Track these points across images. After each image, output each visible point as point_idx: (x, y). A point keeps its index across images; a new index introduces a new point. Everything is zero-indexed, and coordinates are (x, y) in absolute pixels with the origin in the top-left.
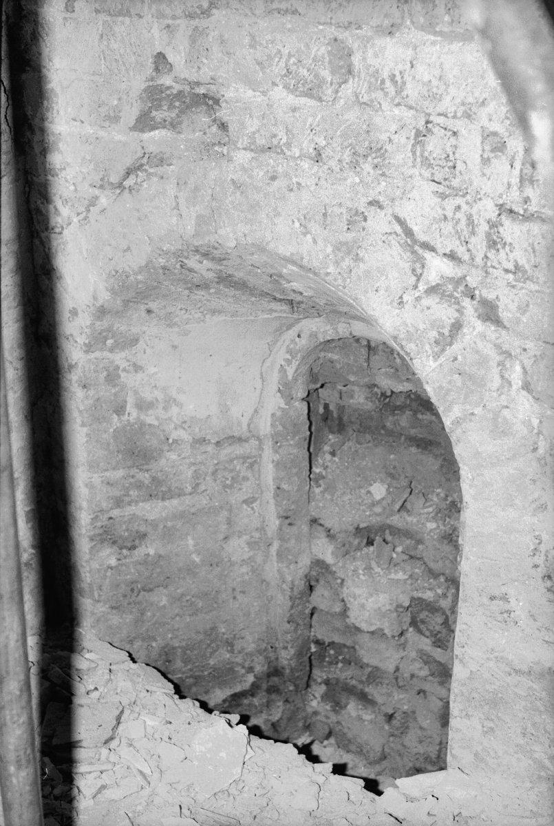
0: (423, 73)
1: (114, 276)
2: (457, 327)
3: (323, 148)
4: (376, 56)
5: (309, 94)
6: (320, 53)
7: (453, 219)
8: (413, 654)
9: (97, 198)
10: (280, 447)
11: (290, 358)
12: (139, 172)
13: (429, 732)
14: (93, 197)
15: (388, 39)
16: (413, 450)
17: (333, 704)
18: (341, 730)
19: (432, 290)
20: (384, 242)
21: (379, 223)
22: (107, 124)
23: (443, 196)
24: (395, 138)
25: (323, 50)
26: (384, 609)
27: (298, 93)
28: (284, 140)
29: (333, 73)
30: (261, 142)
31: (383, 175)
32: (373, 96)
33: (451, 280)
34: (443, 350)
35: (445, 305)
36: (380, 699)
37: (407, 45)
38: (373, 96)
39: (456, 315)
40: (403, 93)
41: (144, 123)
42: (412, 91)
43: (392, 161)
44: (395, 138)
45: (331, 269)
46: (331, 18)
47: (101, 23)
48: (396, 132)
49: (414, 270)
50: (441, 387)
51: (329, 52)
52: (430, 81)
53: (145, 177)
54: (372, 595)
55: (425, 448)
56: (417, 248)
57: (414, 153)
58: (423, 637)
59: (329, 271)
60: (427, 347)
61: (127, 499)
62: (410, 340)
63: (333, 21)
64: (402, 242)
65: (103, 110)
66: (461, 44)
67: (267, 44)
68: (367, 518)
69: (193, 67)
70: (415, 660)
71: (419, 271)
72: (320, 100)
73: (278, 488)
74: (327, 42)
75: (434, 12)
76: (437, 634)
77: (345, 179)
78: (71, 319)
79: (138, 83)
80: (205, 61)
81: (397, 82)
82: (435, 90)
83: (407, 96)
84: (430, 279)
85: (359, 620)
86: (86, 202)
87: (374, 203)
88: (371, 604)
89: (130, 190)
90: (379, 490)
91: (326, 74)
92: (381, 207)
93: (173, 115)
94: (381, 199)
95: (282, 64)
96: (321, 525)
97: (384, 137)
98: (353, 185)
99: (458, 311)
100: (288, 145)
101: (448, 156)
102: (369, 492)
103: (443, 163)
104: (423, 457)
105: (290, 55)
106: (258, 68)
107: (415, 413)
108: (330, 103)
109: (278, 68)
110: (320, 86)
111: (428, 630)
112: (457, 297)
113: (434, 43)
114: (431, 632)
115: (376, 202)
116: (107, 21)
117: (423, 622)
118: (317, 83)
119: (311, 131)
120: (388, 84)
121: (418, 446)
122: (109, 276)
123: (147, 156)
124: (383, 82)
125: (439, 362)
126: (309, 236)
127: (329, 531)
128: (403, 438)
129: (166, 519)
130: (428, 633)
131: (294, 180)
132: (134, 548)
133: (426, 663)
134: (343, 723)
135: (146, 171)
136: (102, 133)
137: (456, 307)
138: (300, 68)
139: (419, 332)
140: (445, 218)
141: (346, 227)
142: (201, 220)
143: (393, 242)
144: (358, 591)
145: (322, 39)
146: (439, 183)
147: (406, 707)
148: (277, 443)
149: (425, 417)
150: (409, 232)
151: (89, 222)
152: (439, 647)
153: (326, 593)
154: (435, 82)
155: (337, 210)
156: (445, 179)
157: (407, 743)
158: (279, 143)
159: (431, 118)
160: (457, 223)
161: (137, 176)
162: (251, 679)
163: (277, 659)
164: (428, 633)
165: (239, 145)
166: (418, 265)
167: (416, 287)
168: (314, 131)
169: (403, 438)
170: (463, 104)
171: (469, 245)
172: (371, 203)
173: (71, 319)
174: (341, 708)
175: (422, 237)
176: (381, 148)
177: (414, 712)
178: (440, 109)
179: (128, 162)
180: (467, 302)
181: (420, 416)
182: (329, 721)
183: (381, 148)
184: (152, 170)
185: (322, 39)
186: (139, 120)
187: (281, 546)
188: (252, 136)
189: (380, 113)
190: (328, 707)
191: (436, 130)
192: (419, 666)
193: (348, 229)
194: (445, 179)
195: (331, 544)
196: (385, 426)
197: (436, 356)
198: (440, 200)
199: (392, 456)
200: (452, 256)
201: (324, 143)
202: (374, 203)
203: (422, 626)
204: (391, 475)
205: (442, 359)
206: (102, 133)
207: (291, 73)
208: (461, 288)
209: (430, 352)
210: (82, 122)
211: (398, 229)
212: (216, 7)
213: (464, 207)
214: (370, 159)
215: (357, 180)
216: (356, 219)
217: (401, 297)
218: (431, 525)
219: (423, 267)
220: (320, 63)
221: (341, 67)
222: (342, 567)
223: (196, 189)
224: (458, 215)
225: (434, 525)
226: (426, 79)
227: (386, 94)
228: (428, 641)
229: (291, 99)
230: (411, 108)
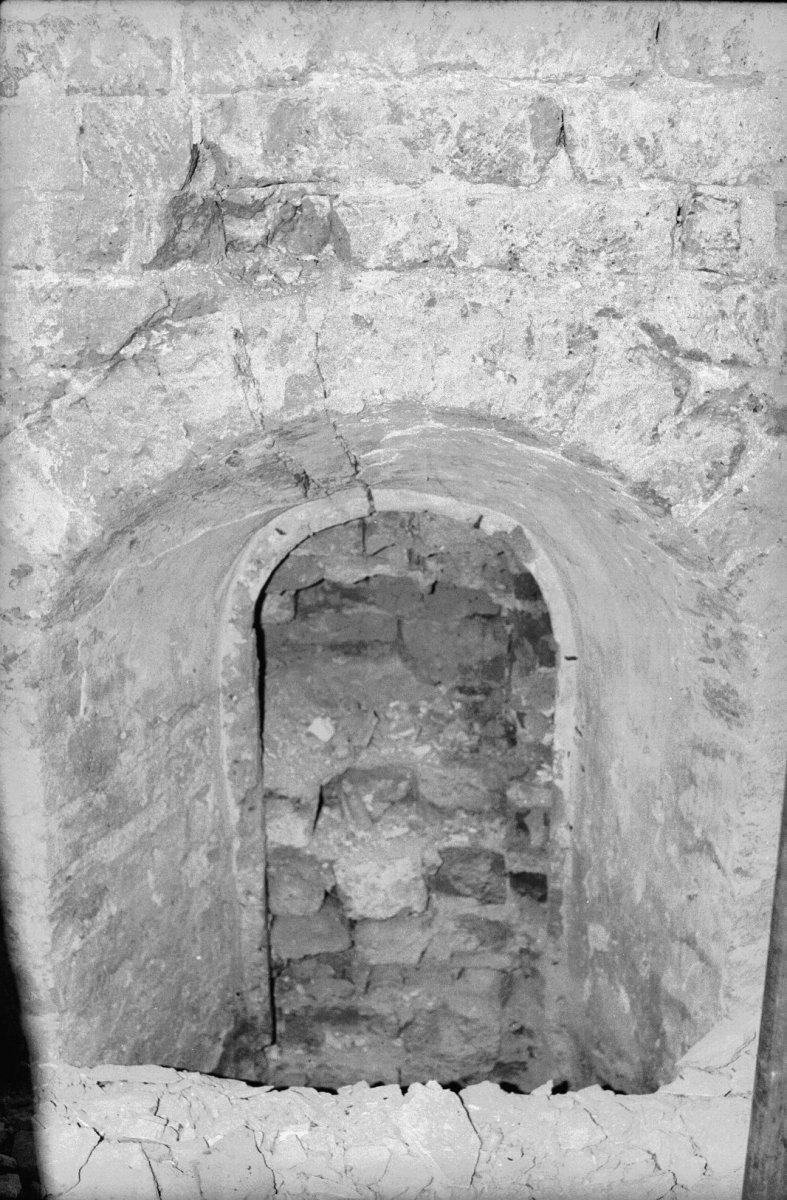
0: (687, 130)
1: (112, 497)
2: (739, 450)
3: (524, 250)
4: (613, 115)
5: (498, 178)
6: (518, 121)
7: (735, 314)
8: (451, 926)
9: (66, 383)
10: (236, 702)
11: (255, 569)
12: (153, 332)
13: (482, 1023)
14: (58, 384)
15: (632, 92)
16: (340, 661)
17: (304, 1045)
18: (326, 1074)
19: (700, 411)
20: (630, 360)
21: (614, 338)
22: (93, 266)
23: (718, 288)
24: (647, 222)
25: (523, 115)
26: (406, 880)
27: (478, 179)
28: (454, 247)
29: (536, 145)
30: (407, 254)
31: (623, 272)
32: (609, 170)
33: (723, 392)
34: (718, 485)
35: (719, 426)
36: (384, 1009)
37: (663, 98)
38: (609, 170)
39: (738, 435)
40: (657, 161)
41: (167, 255)
42: (671, 155)
43: (639, 253)
44: (647, 222)
45: (541, 412)
46: (537, 71)
47: (78, 109)
48: (648, 214)
49: (677, 389)
50: (716, 532)
51: (533, 118)
52: (699, 142)
53: (165, 338)
54: (384, 867)
55: (359, 653)
56: (678, 360)
57: (672, 236)
58: (463, 900)
59: (537, 415)
60: (696, 485)
61: (86, 840)
62: (666, 483)
63: (539, 75)
64: (656, 355)
65: (87, 246)
66: (745, 90)
67: (423, 114)
68: (324, 769)
69: (278, 160)
70: (455, 933)
71: (684, 390)
72: (516, 184)
73: (236, 762)
74: (530, 104)
75: (707, 52)
76: (484, 887)
77: (558, 287)
78: (14, 584)
79: (160, 193)
80: (304, 149)
81: (647, 147)
82: (707, 152)
83: (665, 165)
84: (697, 396)
85: (370, 907)
86: (47, 393)
87: (606, 312)
88: (386, 880)
89: (136, 361)
90: (322, 728)
91: (527, 147)
92: (617, 316)
93: (198, 236)
94: (618, 305)
95: (451, 141)
96: (282, 797)
97: (628, 223)
98: (572, 294)
99: (739, 430)
100: (461, 253)
101: (729, 234)
102: (310, 735)
103: (720, 244)
104: (359, 667)
105: (464, 127)
106: (407, 150)
107: (338, 608)
108: (533, 187)
109: (443, 148)
110: (516, 165)
111: (467, 886)
112: (736, 413)
113: (704, 93)
114: (473, 887)
115: (608, 310)
116: (95, 104)
117: (457, 878)
118: (512, 162)
119: (505, 228)
120: (633, 151)
121: (347, 653)
122: (104, 498)
123: (173, 305)
124: (625, 149)
125: (713, 500)
126: (499, 375)
127: (299, 801)
128: (319, 649)
129: (126, 855)
130: (468, 891)
131: (467, 299)
132: (95, 911)
133: (472, 930)
134: (329, 1064)
135: (168, 327)
136: (77, 281)
137: (735, 425)
138: (483, 143)
139: (683, 468)
140: (723, 314)
141: (566, 351)
142: (295, 384)
143: (644, 358)
144: (359, 870)
145: (521, 101)
146: (716, 272)
147: (430, 1004)
148: (231, 697)
149: (355, 611)
150: (668, 343)
151: (53, 423)
152: (490, 902)
153: (295, 892)
154: (707, 142)
155: (550, 330)
156: (724, 265)
157: (443, 1049)
158: (445, 252)
159: (700, 189)
160: (742, 318)
161: (149, 339)
162: (219, 1049)
163: (245, 1009)
164: (468, 891)
165: (371, 263)
166: (681, 382)
167: (678, 411)
168: (509, 229)
169: (319, 649)
170: (751, 166)
171: (760, 343)
172: (600, 314)
173: (14, 584)
174: (318, 1044)
175: (687, 343)
176: (624, 237)
177: (445, 1006)
178: (717, 174)
179: (143, 313)
180: (748, 417)
181: (348, 612)
182: (304, 1071)
183: (624, 237)
184: (178, 325)
185: (521, 101)
186: (160, 252)
187: (243, 844)
188: (394, 251)
189: (618, 191)
190: (300, 1052)
191: (709, 204)
192: (463, 939)
193: (570, 352)
194: (724, 265)
195: (303, 818)
196: (288, 640)
197: (708, 494)
198: (713, 293)
199: (309, 679)
200: (733, 362)
201: (526, 242)
202: (606, 312)
203: (458, 885)
204: (328, 704)
205: (718, 496)
206: (77, 281)
207: (467, 151)
208: (743, 401)
209: (699, 490)
210: (39, 268)
211: (647, 339)
212: (317, 69)
213: (751, 296)
214: (603, 254)
215: (578, 285)
216: (581, 337)
217: (656, 429)
218: (422, 751)
219: (689, 383)
220: (518, 133)
221: (547, 136)
222: (319, 847)
223: (286, 339)
224: (743, 307)
225: (426, 749)
226: (694, 138)
227: (629, 165)
228: (472, 901)
229: (464, 188)
230: (667, 179)
